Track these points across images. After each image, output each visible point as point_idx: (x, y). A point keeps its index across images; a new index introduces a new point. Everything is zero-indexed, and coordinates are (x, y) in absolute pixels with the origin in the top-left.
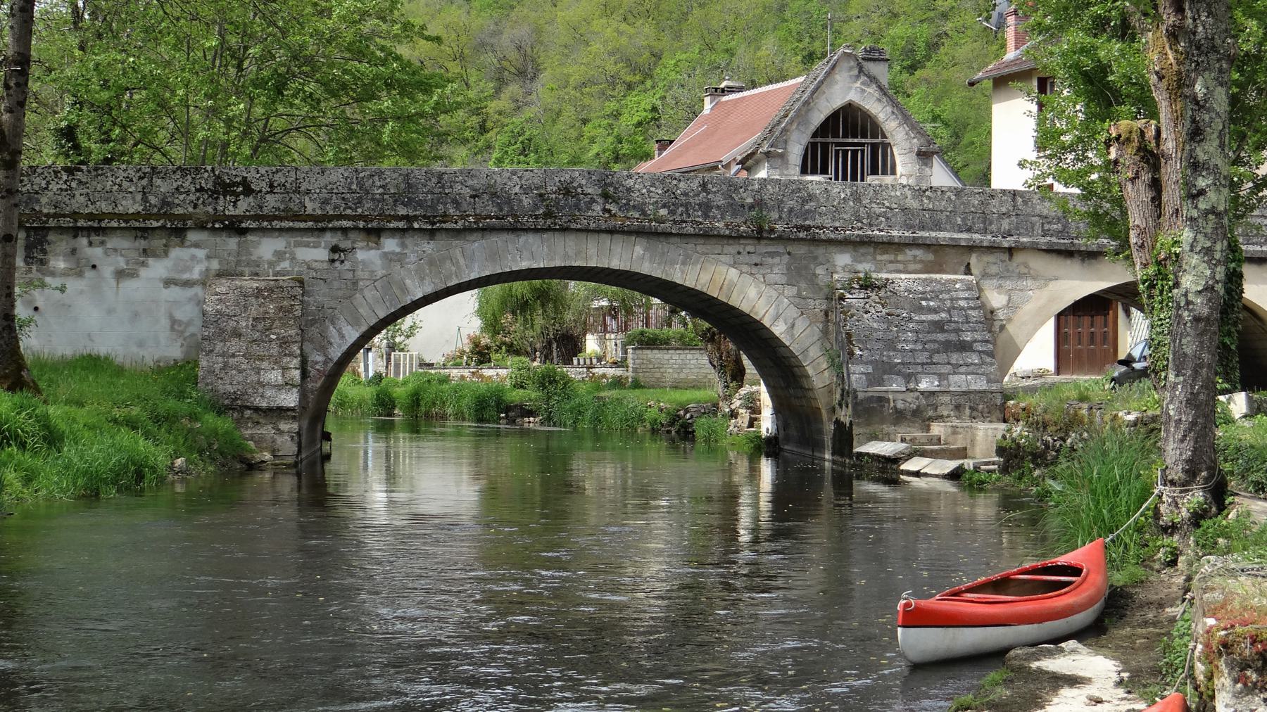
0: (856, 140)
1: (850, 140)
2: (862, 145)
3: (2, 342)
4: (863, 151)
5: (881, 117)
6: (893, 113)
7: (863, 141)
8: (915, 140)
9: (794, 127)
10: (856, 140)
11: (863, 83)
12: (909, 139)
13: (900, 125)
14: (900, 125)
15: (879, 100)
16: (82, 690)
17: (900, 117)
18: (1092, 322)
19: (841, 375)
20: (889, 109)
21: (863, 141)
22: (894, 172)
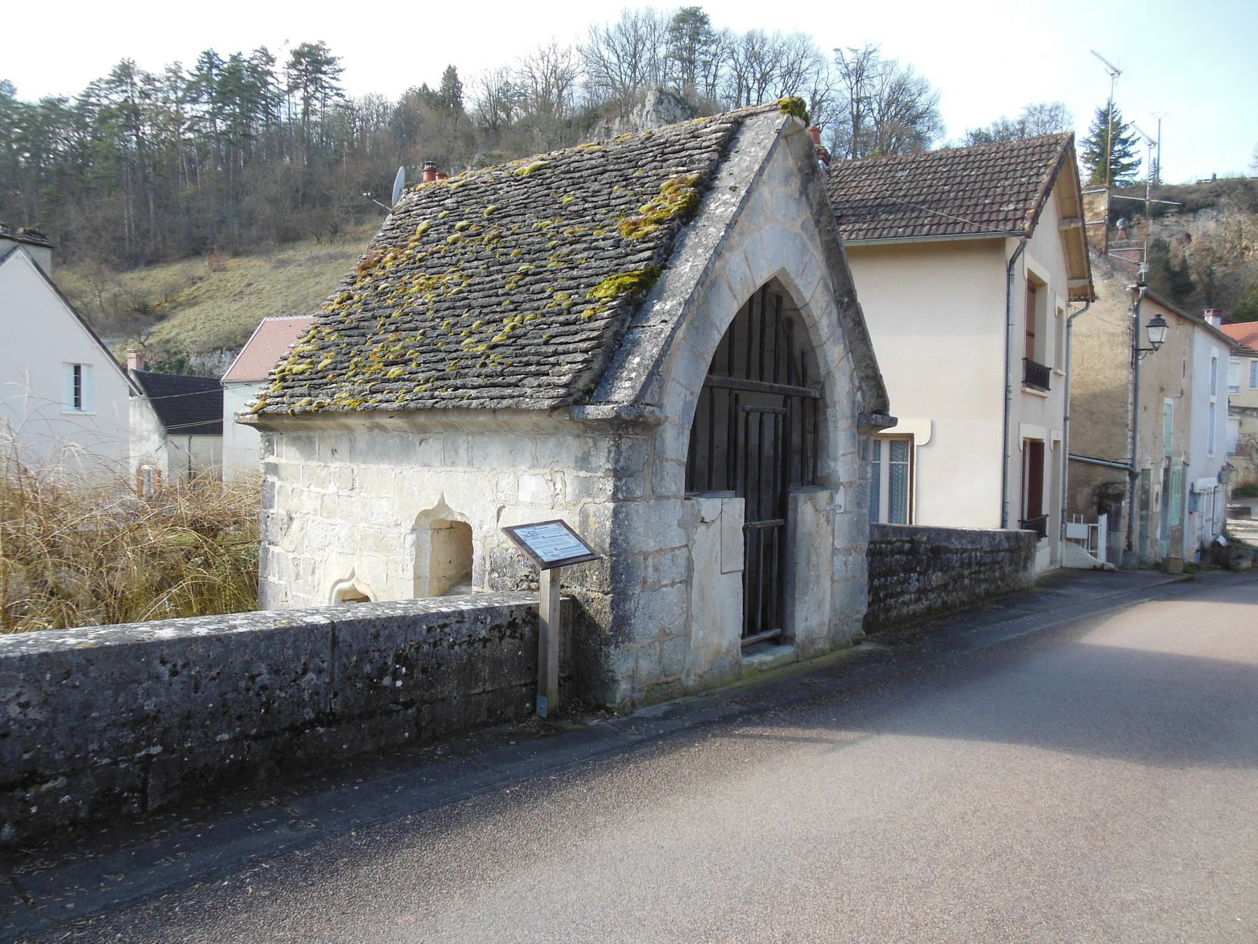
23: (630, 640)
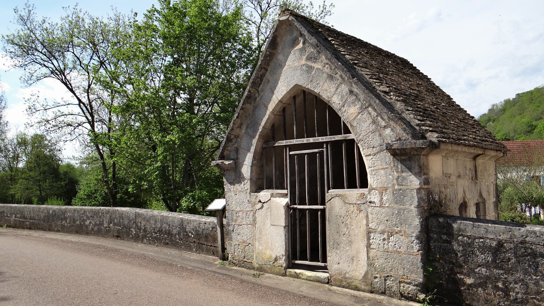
0: (311, 140)
1: (305, 141)
2: (319, 145)
3: (1, 258)
4: (321, 153)
5: (336, 102)
6: (351, 92)
7: (320, 139)
8: (388, 131)
9: (243, 131)
10: (311, 140)
11: (309, 58)
12: (378, 130)
13: (363, 109)
14: (363, 109)
15: (331, 77)
16: (474, 146)
17: (362, 97)
18: (281, 115)
19: (430, 91)
20: (344, 88)
21: (320, 139)
22: (364, 184)
23: (231, 241)
